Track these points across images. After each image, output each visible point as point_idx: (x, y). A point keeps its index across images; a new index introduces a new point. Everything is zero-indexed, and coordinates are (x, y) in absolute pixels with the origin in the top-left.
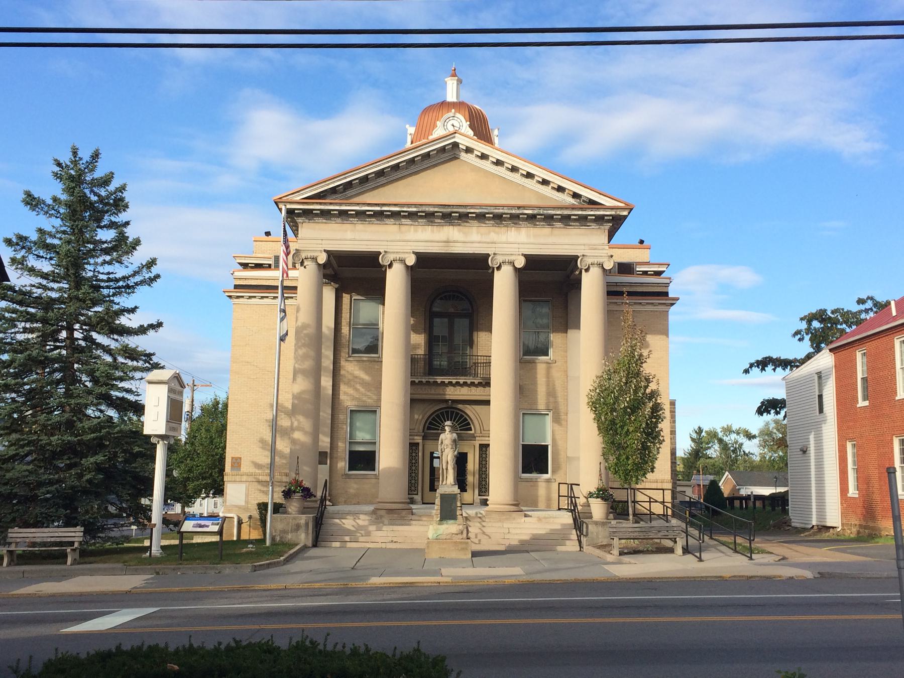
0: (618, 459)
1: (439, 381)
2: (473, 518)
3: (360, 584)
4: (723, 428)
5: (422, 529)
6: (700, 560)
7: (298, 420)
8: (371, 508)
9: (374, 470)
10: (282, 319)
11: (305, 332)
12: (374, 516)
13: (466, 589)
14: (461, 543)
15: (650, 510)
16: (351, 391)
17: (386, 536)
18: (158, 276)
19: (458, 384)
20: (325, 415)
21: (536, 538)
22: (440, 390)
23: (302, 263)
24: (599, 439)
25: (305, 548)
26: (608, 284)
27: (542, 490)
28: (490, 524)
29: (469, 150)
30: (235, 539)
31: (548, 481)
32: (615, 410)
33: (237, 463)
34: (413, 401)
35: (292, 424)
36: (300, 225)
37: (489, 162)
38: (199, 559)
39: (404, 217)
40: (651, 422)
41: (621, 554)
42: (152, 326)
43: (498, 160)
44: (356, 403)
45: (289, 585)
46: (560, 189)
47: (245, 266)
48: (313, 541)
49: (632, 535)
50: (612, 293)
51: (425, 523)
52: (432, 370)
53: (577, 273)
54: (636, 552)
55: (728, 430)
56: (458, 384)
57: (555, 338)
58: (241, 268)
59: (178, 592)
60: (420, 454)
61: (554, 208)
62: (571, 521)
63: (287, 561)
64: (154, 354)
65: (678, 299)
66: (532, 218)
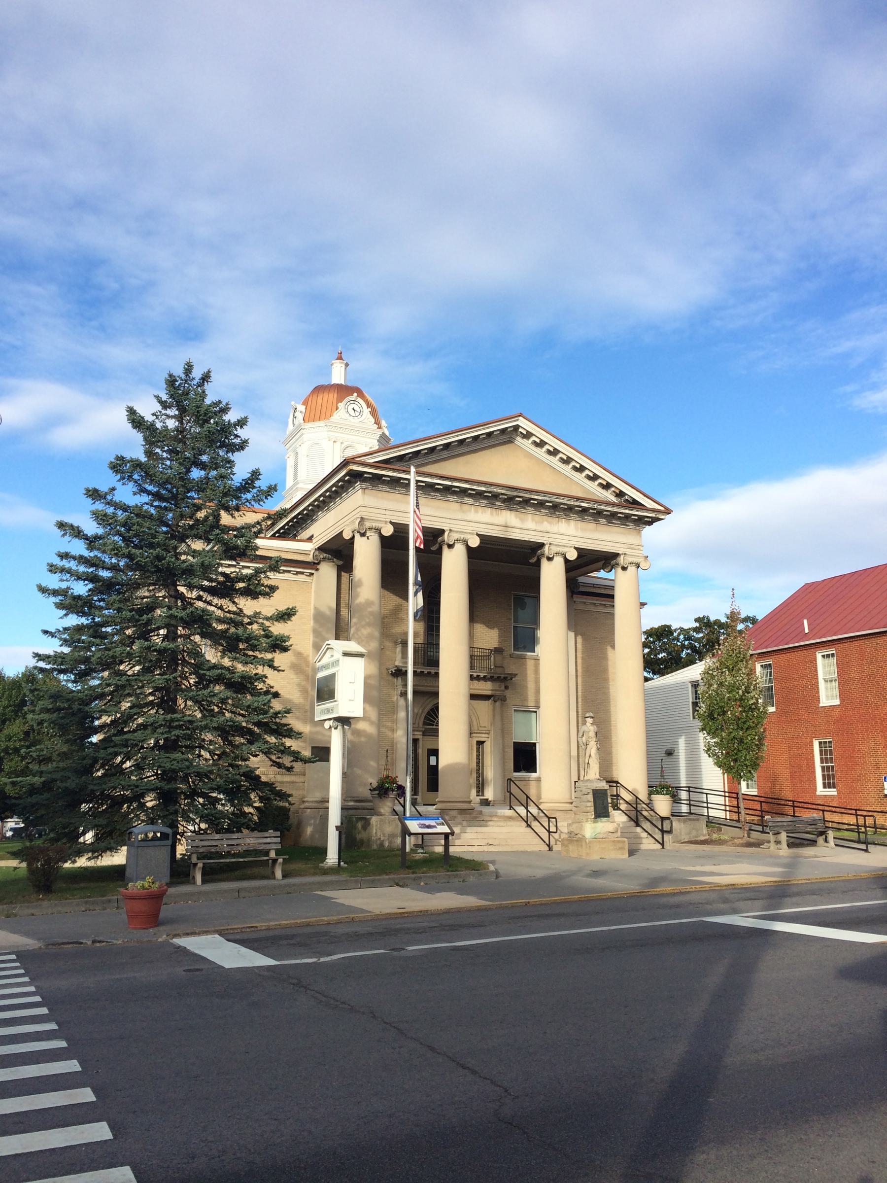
11: (370, 610)
39: (470, 496)
46: (607, 486)
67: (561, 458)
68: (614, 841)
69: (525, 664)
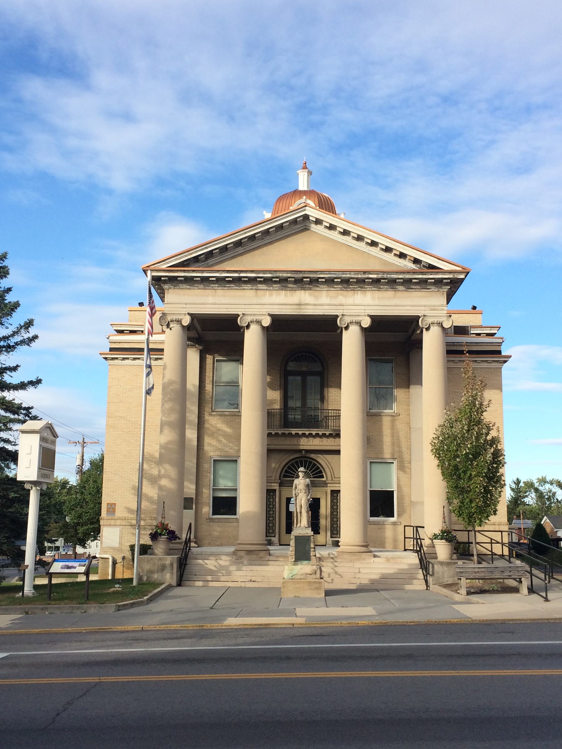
0: (462, 502)
1: (294, 433)
2: (327, 558)
3: (216, 626)
4: (538, 479)
5: (278, 569)
6: (546, 600)
7: (165, 468)
8: (232, 549)
9: (235, 514)
10: (148, 374)
11: (171, 387)
12: (234, 557)
13: (319, 631)
14: (315, 582)
15: (491, 551)
16: (214, 442)
17: (245, 576)
18: (35, 337)
19: (310, 435)
20: (191, 464)
21: (384, 577)
22: (294, 441)
23: (168, 326)
24: (444, 484)
25: (170, 587)
26: (448, 344)
27: (389, 532)
28: (342, 564)
29: (318, 222)
30: (110, 578)
31: (394, 524)
32: (458, 456)
33: (112, 508)
34: (270, 452)
35: (159, 471)
36: (166, 291)
37: (337, 232)
38: (67, 598)
39: (260, 282)
40: (493, 467)
41: (469, 593)
42: (32, 383)
43: (345, 230)
44: (219, 453)
45: (146, 627)
46: (402, 256)
47: (121, 332)
48: (177, 582)
49: (477, 575)
50: (452, 352)
51: (282, 563)
52: (287, 423)
53: (419, 332)
54: (482, 592)
55: (543, 481)
56: (310, 435)
57: (399, 393)
58: (116, 333)
59: (38, 634)
60: (277, 499)
61: (397, 273)
62: (417, 561)
63: (150, 600)
64: (32, 408)
65: (510, 357)
66: (376, 282)
67: (353, 237)
68: (309, 582)
69: (381, 421)
